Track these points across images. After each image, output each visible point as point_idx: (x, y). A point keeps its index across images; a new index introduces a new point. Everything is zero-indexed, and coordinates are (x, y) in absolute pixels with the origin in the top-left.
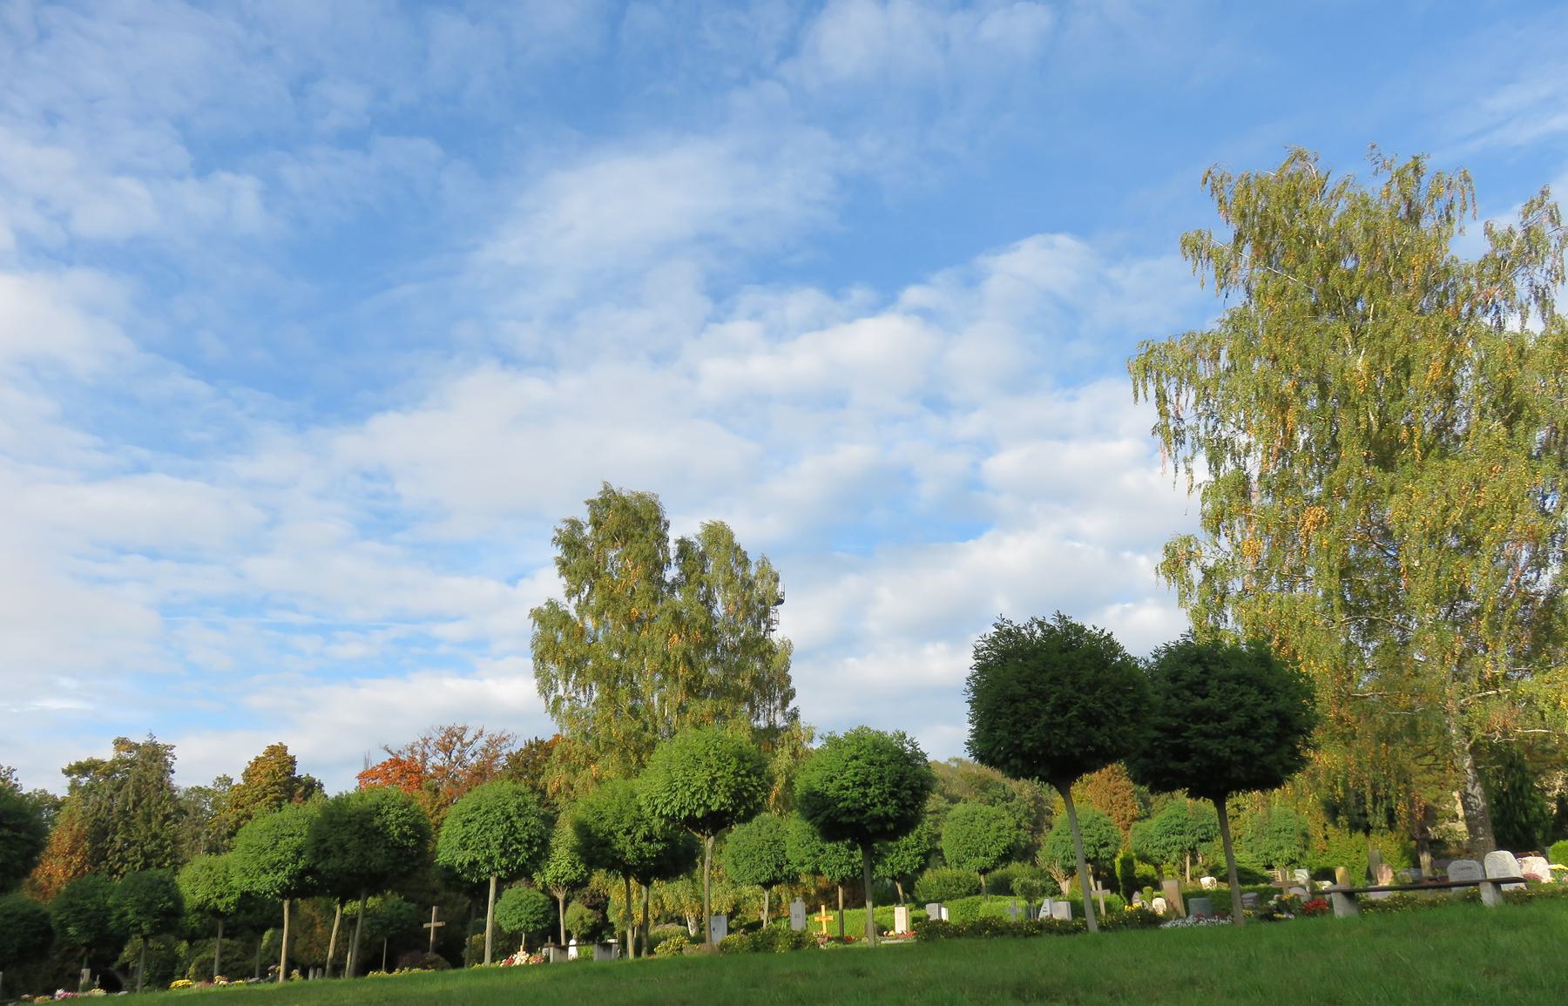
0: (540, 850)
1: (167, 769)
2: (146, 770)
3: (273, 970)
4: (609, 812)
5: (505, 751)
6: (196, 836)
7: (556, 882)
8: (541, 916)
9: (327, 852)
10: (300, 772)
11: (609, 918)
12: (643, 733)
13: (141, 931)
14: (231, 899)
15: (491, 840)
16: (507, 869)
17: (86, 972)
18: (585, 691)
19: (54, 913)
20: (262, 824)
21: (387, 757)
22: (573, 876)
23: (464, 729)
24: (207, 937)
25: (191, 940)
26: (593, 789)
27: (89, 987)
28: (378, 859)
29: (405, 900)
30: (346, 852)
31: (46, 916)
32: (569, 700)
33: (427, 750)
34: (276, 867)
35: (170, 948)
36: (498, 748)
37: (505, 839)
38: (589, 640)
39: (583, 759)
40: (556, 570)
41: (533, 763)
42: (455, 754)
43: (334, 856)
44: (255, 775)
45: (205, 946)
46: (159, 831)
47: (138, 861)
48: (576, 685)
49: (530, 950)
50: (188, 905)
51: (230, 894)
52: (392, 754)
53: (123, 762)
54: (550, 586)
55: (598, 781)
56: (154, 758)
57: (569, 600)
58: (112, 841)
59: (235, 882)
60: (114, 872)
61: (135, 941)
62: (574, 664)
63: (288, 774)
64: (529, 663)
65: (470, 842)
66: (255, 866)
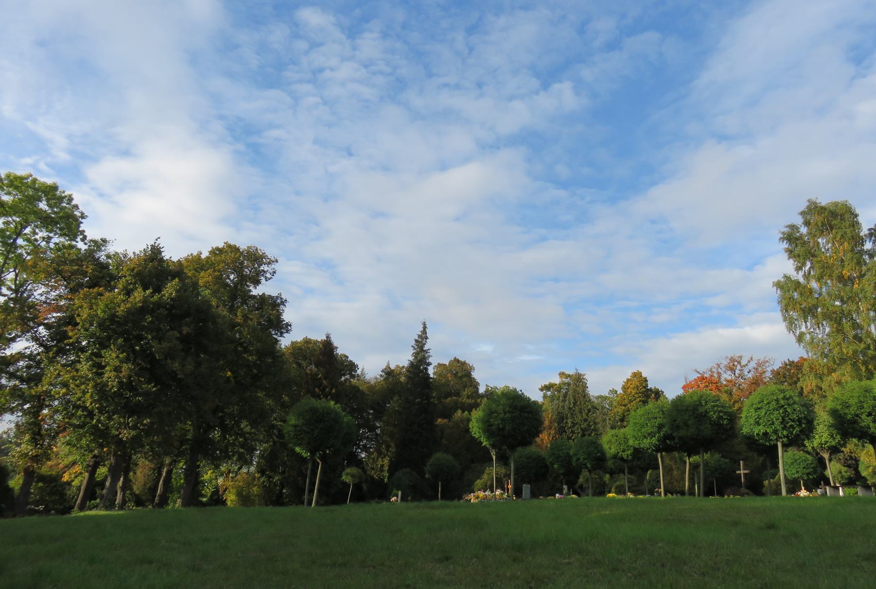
0: (807, 426)
1: (585, 387)
2: (577, 387)
3: (658, 491)
4: (852, 402)
5: (769, 369)
6: (604, 420)
7: (821, 447)
8: (812, 470)
9: (678, 427)
10: (651, 385)
11: (861, 473)
12: (867, 351)
13: (587, 468)
14: (629, 452)
15: (774, 419)
16: (787, 437)
17: (565, 487)
18: (819, 327)
19: (547, 457)
20: (638, 414)
21: (697, 375)
22: (833, 443)
23: (741, 357)
24: (618, 473)
25: (611, 474)
26: (837, 389)
27: (568, 494)
28: (707, 430)
29: (721, 457)
30: (688, 426)
31: (544, 459)
32: (809, 334)
33: (720, 370)
34: (651, 435)
35: (601, 478)
36: (764, 367)
37: (783, 419)
38: (816, 296)
39: (825, 371)
40: (786, 255)
41: (790, 375)
42: (737, 372)
43: (682, 429)
44: (628, 388)
45: (618, 478)
46: (587, 418)
47: (579, 433)
48: (812, 326)
49: (808, 489)
50: (608, 455)
51: (628, 450)
52: (700, 374)
53: (564, 384)
54: (785, 267)
55: (839, 383)
56: (578, 380)
57: (798, 273)
58: (566, 422)
59: (631, 442)
60: (570, 438)
61: (584, 473)
62: (809, 312)
63: (645, 387)
64: (779, 315)
65: (761, 421)
66: (640, 434)
